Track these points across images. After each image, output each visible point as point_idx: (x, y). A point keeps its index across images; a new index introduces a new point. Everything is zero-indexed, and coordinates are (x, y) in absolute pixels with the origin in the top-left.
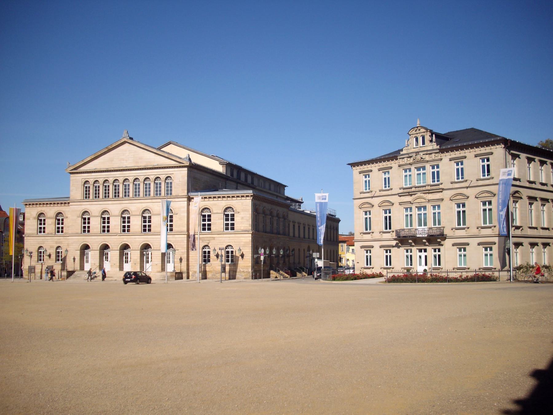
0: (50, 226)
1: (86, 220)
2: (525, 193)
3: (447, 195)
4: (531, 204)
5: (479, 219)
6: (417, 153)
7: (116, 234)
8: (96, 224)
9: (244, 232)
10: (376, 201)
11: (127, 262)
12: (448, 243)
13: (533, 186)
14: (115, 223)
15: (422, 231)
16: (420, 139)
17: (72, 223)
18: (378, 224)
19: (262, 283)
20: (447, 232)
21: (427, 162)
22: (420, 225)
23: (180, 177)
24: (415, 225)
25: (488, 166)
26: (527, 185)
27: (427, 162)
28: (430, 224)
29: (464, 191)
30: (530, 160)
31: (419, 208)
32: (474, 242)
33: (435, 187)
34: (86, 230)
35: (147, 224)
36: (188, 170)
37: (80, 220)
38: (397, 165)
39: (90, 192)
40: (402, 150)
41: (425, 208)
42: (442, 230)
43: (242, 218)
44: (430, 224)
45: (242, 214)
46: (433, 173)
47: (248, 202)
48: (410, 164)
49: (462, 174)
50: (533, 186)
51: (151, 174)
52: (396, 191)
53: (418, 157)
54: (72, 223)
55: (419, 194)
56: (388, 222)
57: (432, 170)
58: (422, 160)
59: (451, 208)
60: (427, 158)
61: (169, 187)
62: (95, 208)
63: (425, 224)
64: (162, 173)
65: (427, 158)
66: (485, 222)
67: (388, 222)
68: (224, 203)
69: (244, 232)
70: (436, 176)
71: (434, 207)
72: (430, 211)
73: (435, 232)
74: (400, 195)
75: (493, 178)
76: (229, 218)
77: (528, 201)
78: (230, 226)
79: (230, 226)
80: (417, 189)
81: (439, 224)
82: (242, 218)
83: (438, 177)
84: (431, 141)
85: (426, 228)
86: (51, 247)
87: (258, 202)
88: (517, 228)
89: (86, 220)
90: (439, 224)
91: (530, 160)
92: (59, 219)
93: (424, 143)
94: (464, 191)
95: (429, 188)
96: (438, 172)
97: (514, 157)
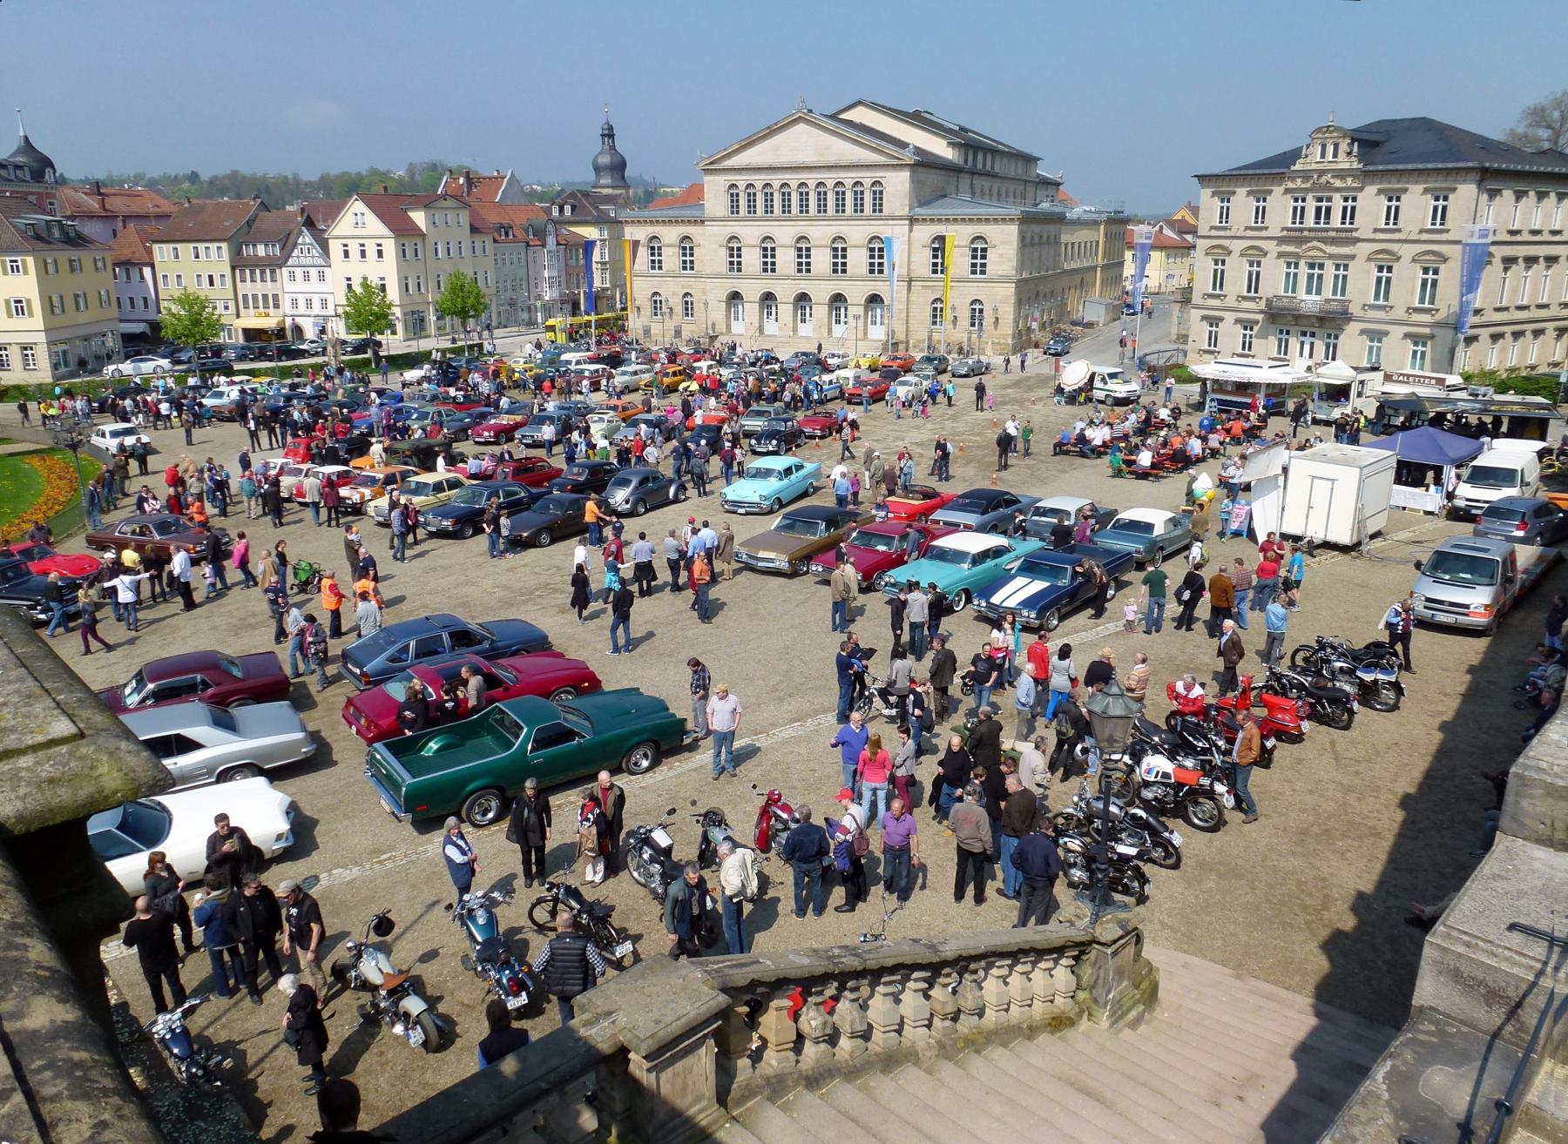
0: (671, 258)
1: (734, 252)
2: (1499, 252)
3: (1363, 250)
4: (1506, 270)
5: (1412, 294)
6: (1322, 172)
7: (787, 278)
8: (752, 259)
9: (1003, 280)
10: (1237, 246)
11: (803, 321)
12: (1352, 329)
13: (1518, 238)
14: (786, 259)
15: (1309, 302)
16: (1330, 149)
17: (710, 253)
18: (1236, 280)
19: (1118, 481)
20: (1355, 309)
21: (1338, 190)
22: (1309, 292)
23: (898, 185)
24: (1302, 294)
25: (1444, 208)
26: (1508, 238)
27: (1338, 190)
28: (1327, 292)
29: (1394, 247)
30: (1519, 195)
31: (1312, 266)
32: (1230, 317)
33: (1344, 235)
34: (735, 265)
35: (877, 261)
36: (913, 180)
37: (724, 252)
38: (1282, 189)
39: (741, 203)
40: (1295, 155)
41: (1321, 266)
42: (1345, 304)
43: (1001, 256)
44: (1327, 292)
45: (1000, 250)
46: (1345, 209)
47: (1012, 231)
48: (1307, 190)
49: (1396, 218)
50: (1518, 238)
51: (848, 178)
52: (1274, 231)
53: (1323, 179)
54: (710, 253)
55: (1315, 243)
56: (1254, 282)
57: (1342, 203)
58: (1328, 187)
59: (1368, 272)
60: (1338, 183)
61: (878, 198)
62: (750, 233)
63: (1319, 292)
64: (867, 178)
65: (1338, 183)
66: (1422, 301)
67: (1254, 282)
68: (970, 230)
69: (1003, 280)
70: (1349, 214)
71: (1338, 267)
72: (1330, 271)
73: (1334, 306)
74: (1281, 240)
75: (1448, 231)
76: (979, 252)
77: (1501, 266)
78: (979, 268)
79: (979, 268)
80: (1313, 234)
81: (1343, 294)
82: (1001, 256)
83: (1352, 217)
84: (1349, 154)
85: (1318, 298)
86: (674, 294)
87: (1024, 227)
88: (1477, 312)
89: (734, 252)
90: (1343, 294)
91: (1519, 195)
92: (687, 247)
93: (1335, 155)
94: (1394, 247)
95: (1333, 234)
96: (1353, 208)
97: (1493, 194)
